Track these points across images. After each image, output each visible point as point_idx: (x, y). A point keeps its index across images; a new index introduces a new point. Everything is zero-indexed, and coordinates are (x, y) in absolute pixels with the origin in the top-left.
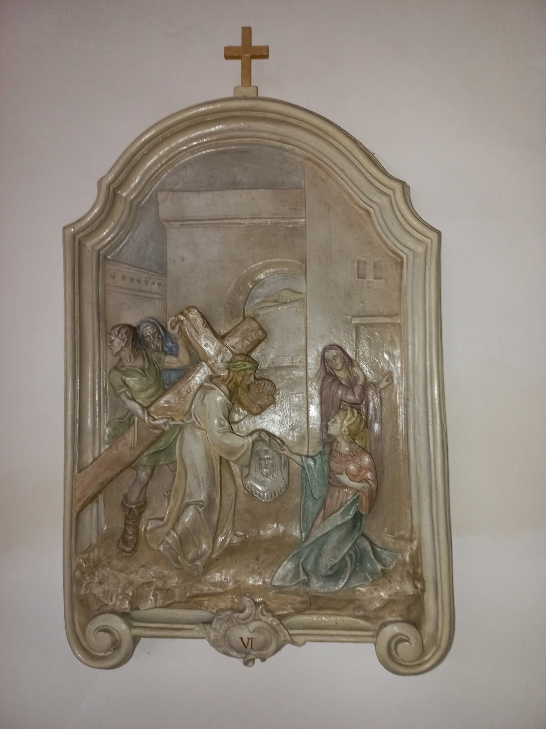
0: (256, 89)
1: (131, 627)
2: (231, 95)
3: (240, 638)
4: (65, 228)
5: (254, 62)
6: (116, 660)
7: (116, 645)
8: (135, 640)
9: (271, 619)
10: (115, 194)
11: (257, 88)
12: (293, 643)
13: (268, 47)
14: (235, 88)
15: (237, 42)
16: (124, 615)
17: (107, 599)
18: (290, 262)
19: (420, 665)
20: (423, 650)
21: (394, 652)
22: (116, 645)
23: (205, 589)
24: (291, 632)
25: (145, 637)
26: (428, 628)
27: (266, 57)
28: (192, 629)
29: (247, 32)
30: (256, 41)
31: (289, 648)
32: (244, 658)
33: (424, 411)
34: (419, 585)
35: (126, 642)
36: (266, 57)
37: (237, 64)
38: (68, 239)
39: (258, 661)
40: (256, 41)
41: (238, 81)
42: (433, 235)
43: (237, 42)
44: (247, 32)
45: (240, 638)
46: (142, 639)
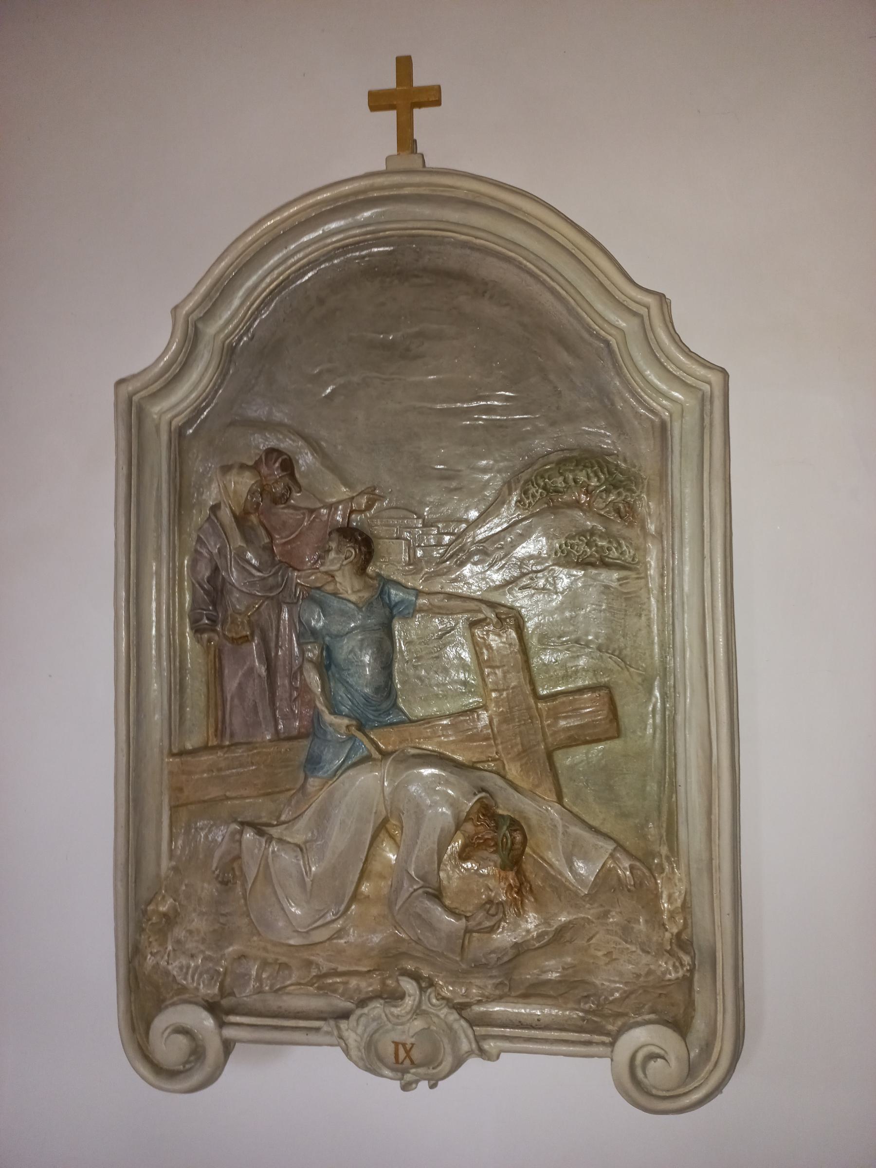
0: (421, 156)
1: (221, 1024)
2: (383, 167)
3: (393, 1042)
4: (120, 383)
5: (416, 111)
6: (196, 1078)
7: (197, 1053)
8: (228, 1046)
9: (445, 1010)
10: (197, 333)
11: (423, 156)
12: (483, 1053)
13: (439, 87)
14: (388, 159)
15: (389, 81)
16: (212, 1008)
17: (185, 979)
18: (153, 567)
19: (685, 1094)
20: (692, 1070)
21: (640, 1074)
22: (197, 1053)
23: (657, 745)
24: (481, 1030)
25: (241, 1041)
26: (700, 1025)
27: (437, 103)
28: (317, 1029)
29: (404, 65)
30: (420, 79)
31: (474, 1064)
32: (401, 1079)
33: (701, 667)
34: (686, 959)
35: (213, 1046)
36: (437, 103)
37: (391, 116)
38: (123, 406)
39: (424, 1085)
40: (420, 79)
41: (393, 149)
42: (715, 378)
43: (389, 81)
44: (404, 65)
45: (393, 1042)
46: (237, 1045)
